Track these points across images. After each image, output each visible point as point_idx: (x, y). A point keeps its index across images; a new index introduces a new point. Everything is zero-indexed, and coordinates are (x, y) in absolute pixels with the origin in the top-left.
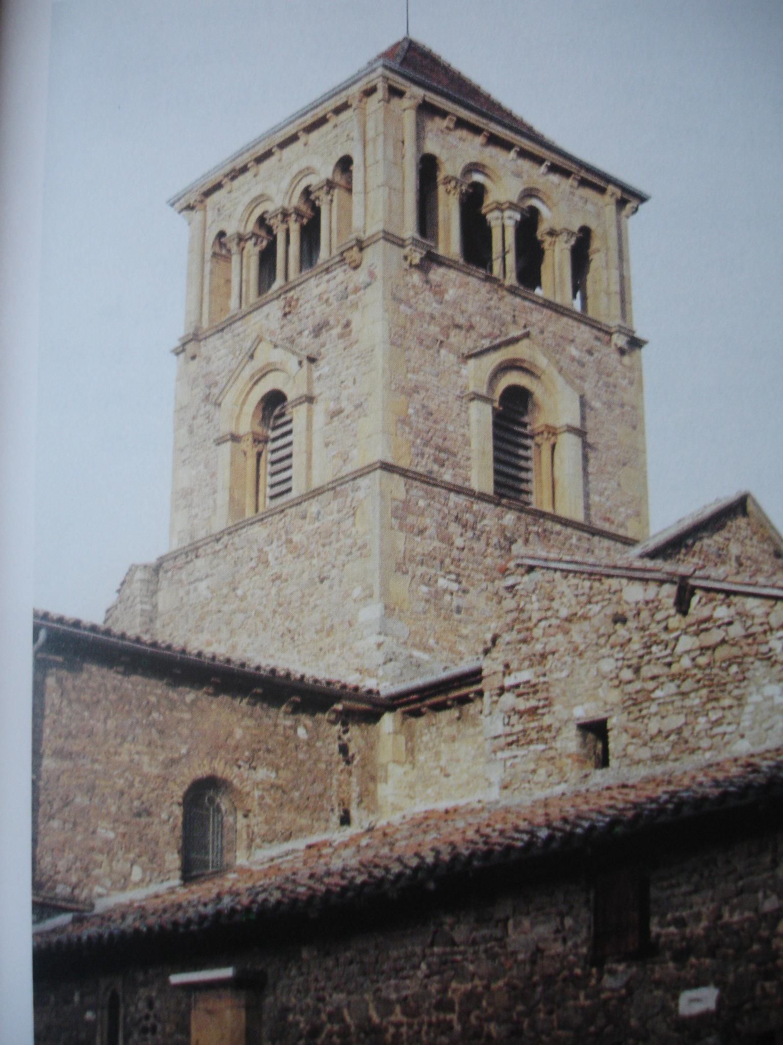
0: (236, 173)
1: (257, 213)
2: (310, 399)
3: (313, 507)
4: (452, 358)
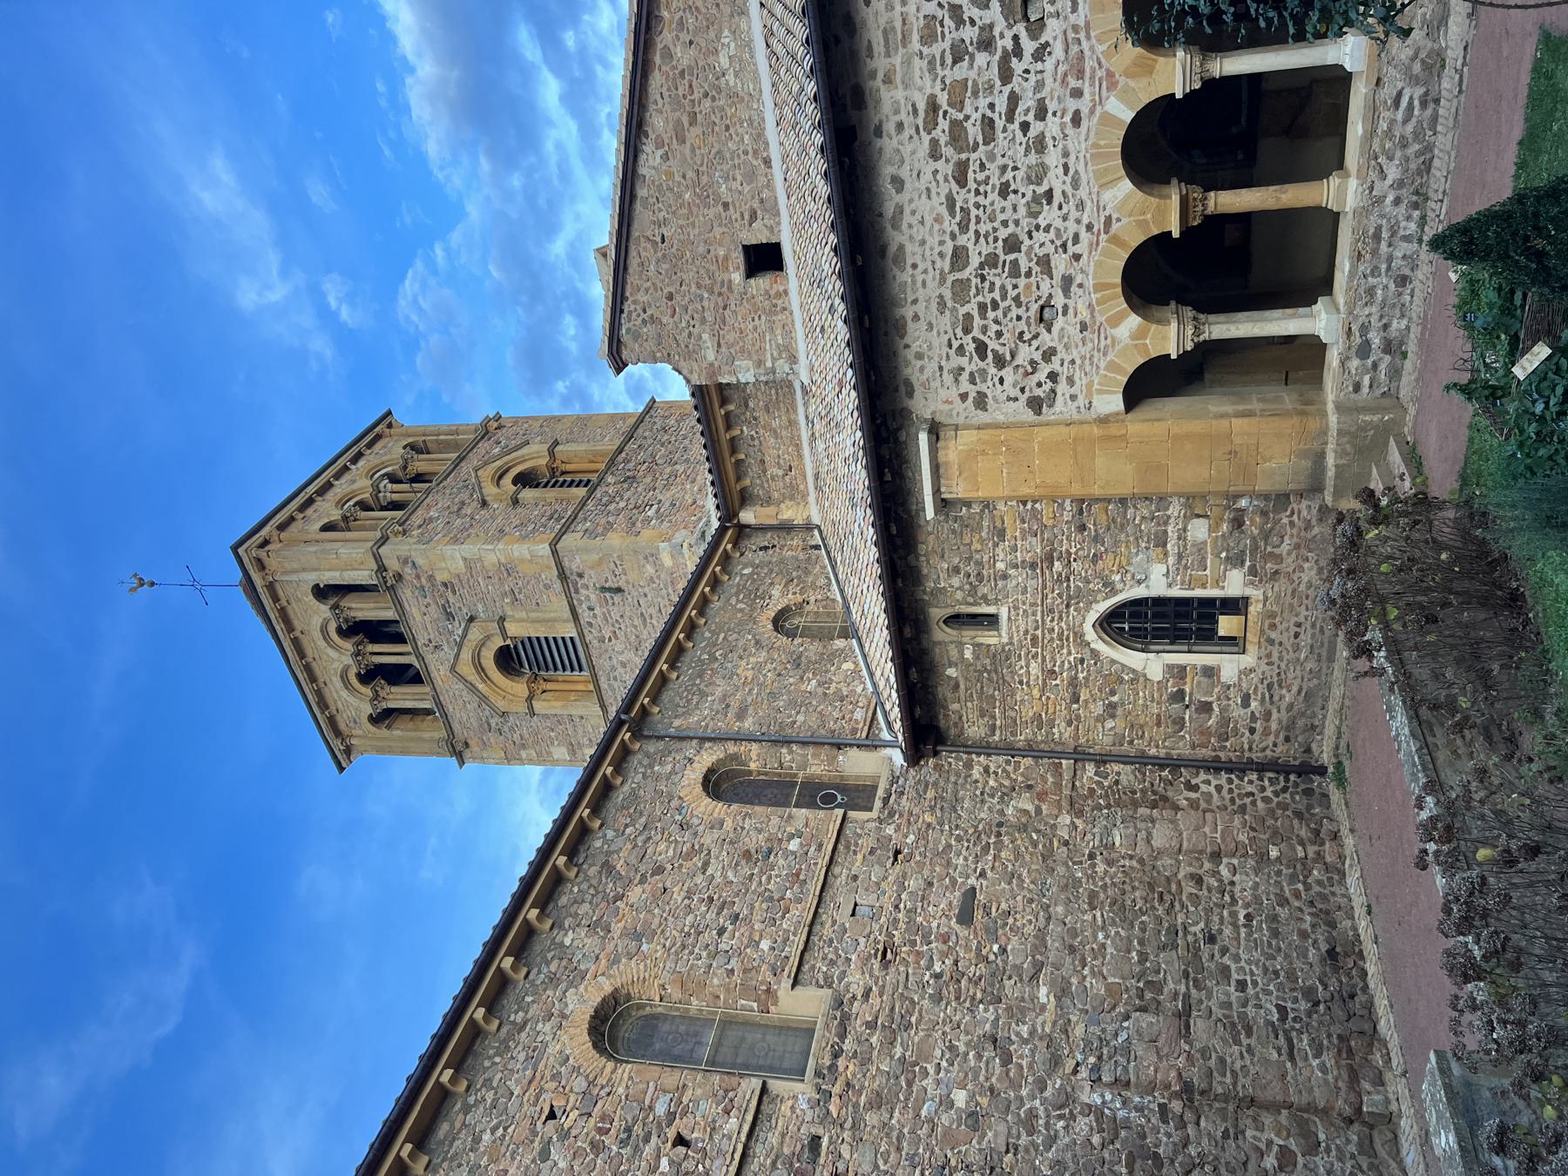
1: (354, 681)
2: (502, 619)
3: (585, 616)
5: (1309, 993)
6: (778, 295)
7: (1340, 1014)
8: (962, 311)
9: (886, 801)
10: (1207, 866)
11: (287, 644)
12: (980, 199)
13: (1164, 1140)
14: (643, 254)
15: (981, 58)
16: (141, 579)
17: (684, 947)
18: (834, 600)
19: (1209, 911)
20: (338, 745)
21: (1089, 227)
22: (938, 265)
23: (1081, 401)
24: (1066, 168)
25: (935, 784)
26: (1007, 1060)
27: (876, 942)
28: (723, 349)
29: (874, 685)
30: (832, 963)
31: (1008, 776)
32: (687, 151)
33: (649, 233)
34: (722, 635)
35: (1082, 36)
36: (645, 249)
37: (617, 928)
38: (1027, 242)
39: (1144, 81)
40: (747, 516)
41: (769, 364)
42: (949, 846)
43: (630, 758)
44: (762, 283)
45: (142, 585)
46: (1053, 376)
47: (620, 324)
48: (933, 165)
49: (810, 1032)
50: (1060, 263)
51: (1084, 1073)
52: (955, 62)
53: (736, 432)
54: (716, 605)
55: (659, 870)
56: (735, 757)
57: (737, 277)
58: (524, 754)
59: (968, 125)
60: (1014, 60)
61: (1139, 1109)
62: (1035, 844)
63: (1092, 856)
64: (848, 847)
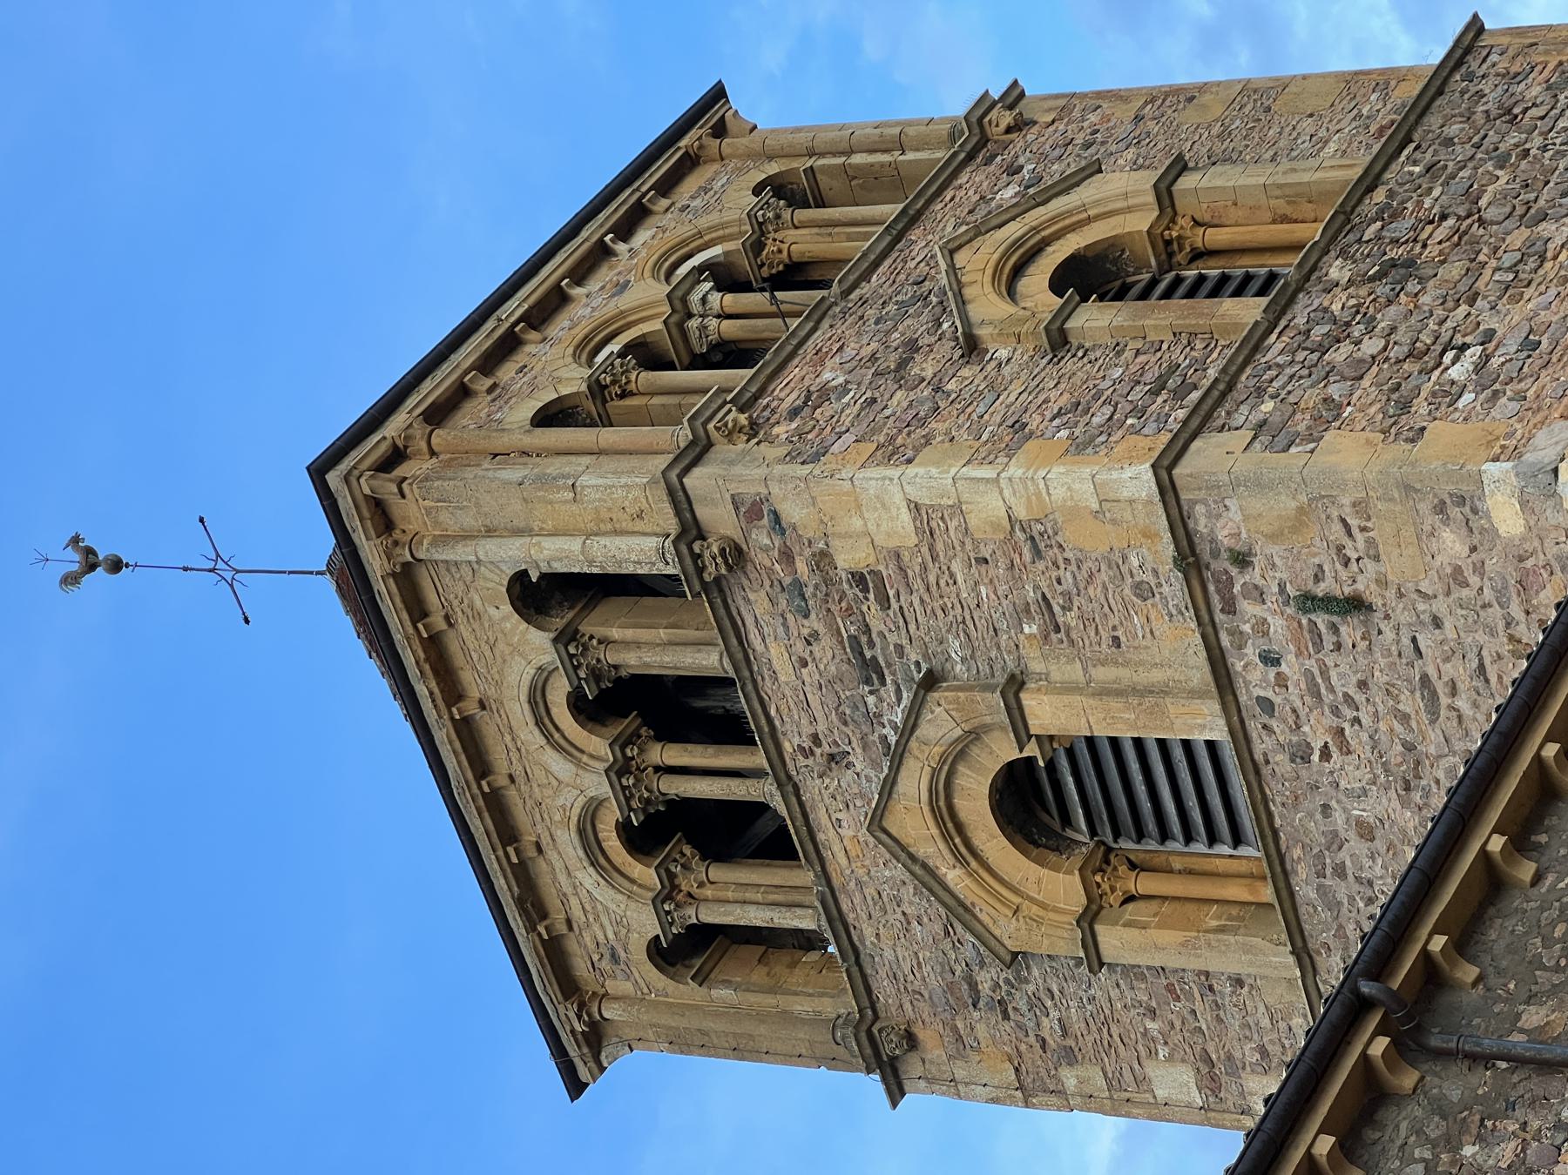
11: (443, 735)
16: (89, 551)
20: (567, 1017)
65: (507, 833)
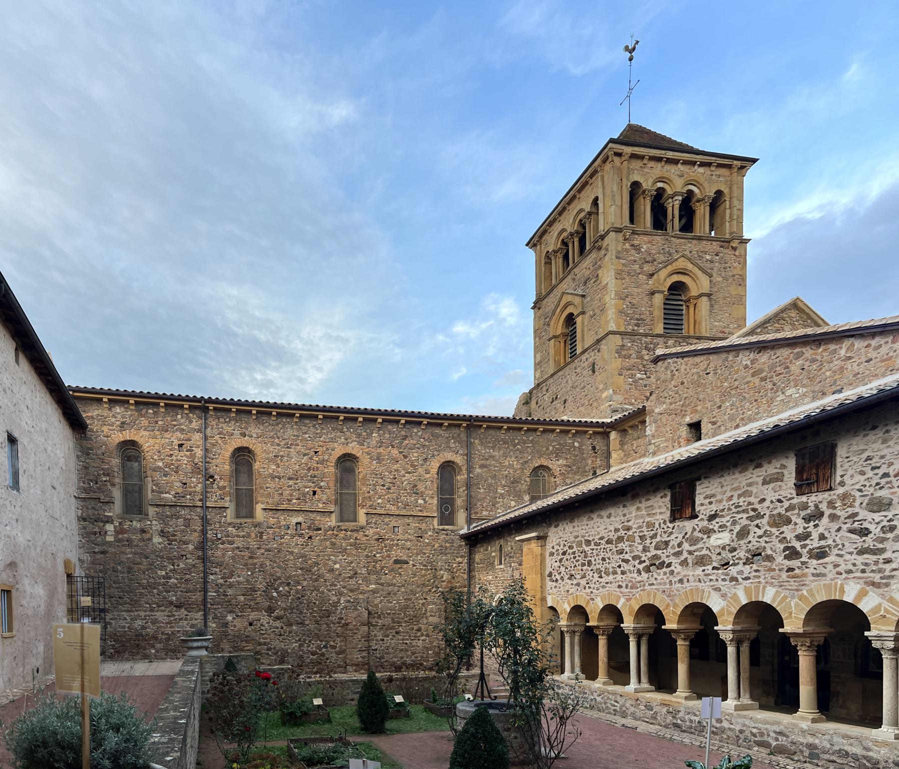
0: (551, 224)
4: (645, 277)
5: (382, 657)
6: (679, 443)
7: (377, 664)
8: (574, 545)
9: (443, 530)
10: (425, 633)
11: (572, 193)
12: (602, 550)
13: (333, 618)
14: (702, 364)
15: (640, 548)
16: (634, 49)
17: (376, 475)
18: (556, 489)
19: (408, 633)
20: (536, 239)
21: (592, 592)
22: (587, 535)
23: (551, 591)
24: (607, 583)
25: (453, 546)
26: (350, 578)
27: (385, 536)
28: (660, 416)
29: (499, 517)
30: (376, 523)
31: (457, 571)
32: (748, 379)
33: (711, 365)
34: (530, 445)
35: (642, 588)
36: (704, 365)
37: (381, 450)
38: (590, 569)
39: (628, 612)
40: (613, 435)
41: (653, 441)
42: (425, 554)
43: (457, 428)
44: (684, 432)
45: (630, 53)
46: (557, 581)
47: (672, 358)
48: (613, 530)
49: (355, 521)
50: (583, 582)
51: (349, 598)
52: (640, 536)
53: (629, 430)
54: (552, 436)
55: (405, 457)
56: (461, 470)
57: (688, 420)
58: (537, 339)
59: (622, 544)
60: (638, 561)
61: (341, 612)
62: (428, 581)
63: (425, 599)
64: (421, 520)
65: (560, 214)
